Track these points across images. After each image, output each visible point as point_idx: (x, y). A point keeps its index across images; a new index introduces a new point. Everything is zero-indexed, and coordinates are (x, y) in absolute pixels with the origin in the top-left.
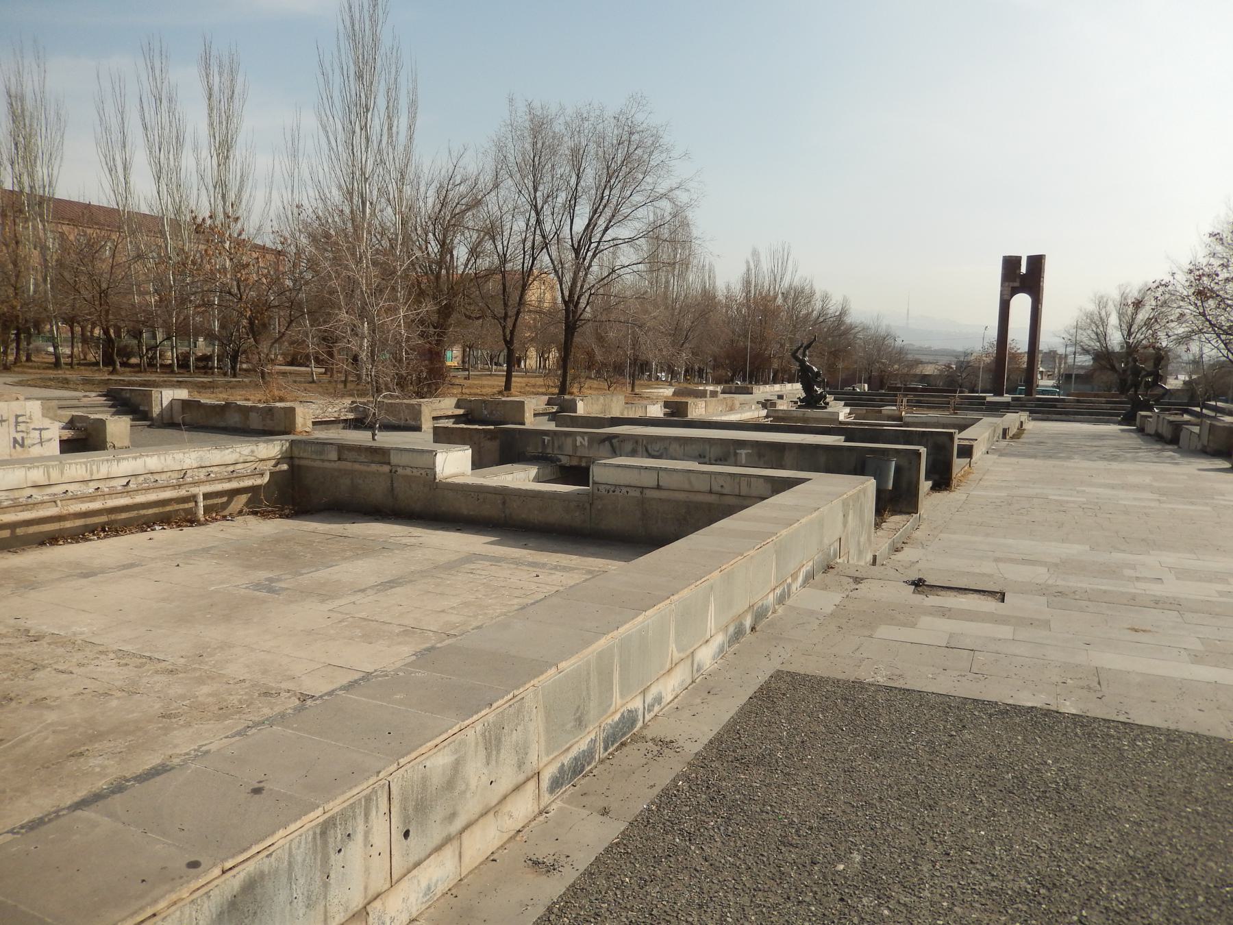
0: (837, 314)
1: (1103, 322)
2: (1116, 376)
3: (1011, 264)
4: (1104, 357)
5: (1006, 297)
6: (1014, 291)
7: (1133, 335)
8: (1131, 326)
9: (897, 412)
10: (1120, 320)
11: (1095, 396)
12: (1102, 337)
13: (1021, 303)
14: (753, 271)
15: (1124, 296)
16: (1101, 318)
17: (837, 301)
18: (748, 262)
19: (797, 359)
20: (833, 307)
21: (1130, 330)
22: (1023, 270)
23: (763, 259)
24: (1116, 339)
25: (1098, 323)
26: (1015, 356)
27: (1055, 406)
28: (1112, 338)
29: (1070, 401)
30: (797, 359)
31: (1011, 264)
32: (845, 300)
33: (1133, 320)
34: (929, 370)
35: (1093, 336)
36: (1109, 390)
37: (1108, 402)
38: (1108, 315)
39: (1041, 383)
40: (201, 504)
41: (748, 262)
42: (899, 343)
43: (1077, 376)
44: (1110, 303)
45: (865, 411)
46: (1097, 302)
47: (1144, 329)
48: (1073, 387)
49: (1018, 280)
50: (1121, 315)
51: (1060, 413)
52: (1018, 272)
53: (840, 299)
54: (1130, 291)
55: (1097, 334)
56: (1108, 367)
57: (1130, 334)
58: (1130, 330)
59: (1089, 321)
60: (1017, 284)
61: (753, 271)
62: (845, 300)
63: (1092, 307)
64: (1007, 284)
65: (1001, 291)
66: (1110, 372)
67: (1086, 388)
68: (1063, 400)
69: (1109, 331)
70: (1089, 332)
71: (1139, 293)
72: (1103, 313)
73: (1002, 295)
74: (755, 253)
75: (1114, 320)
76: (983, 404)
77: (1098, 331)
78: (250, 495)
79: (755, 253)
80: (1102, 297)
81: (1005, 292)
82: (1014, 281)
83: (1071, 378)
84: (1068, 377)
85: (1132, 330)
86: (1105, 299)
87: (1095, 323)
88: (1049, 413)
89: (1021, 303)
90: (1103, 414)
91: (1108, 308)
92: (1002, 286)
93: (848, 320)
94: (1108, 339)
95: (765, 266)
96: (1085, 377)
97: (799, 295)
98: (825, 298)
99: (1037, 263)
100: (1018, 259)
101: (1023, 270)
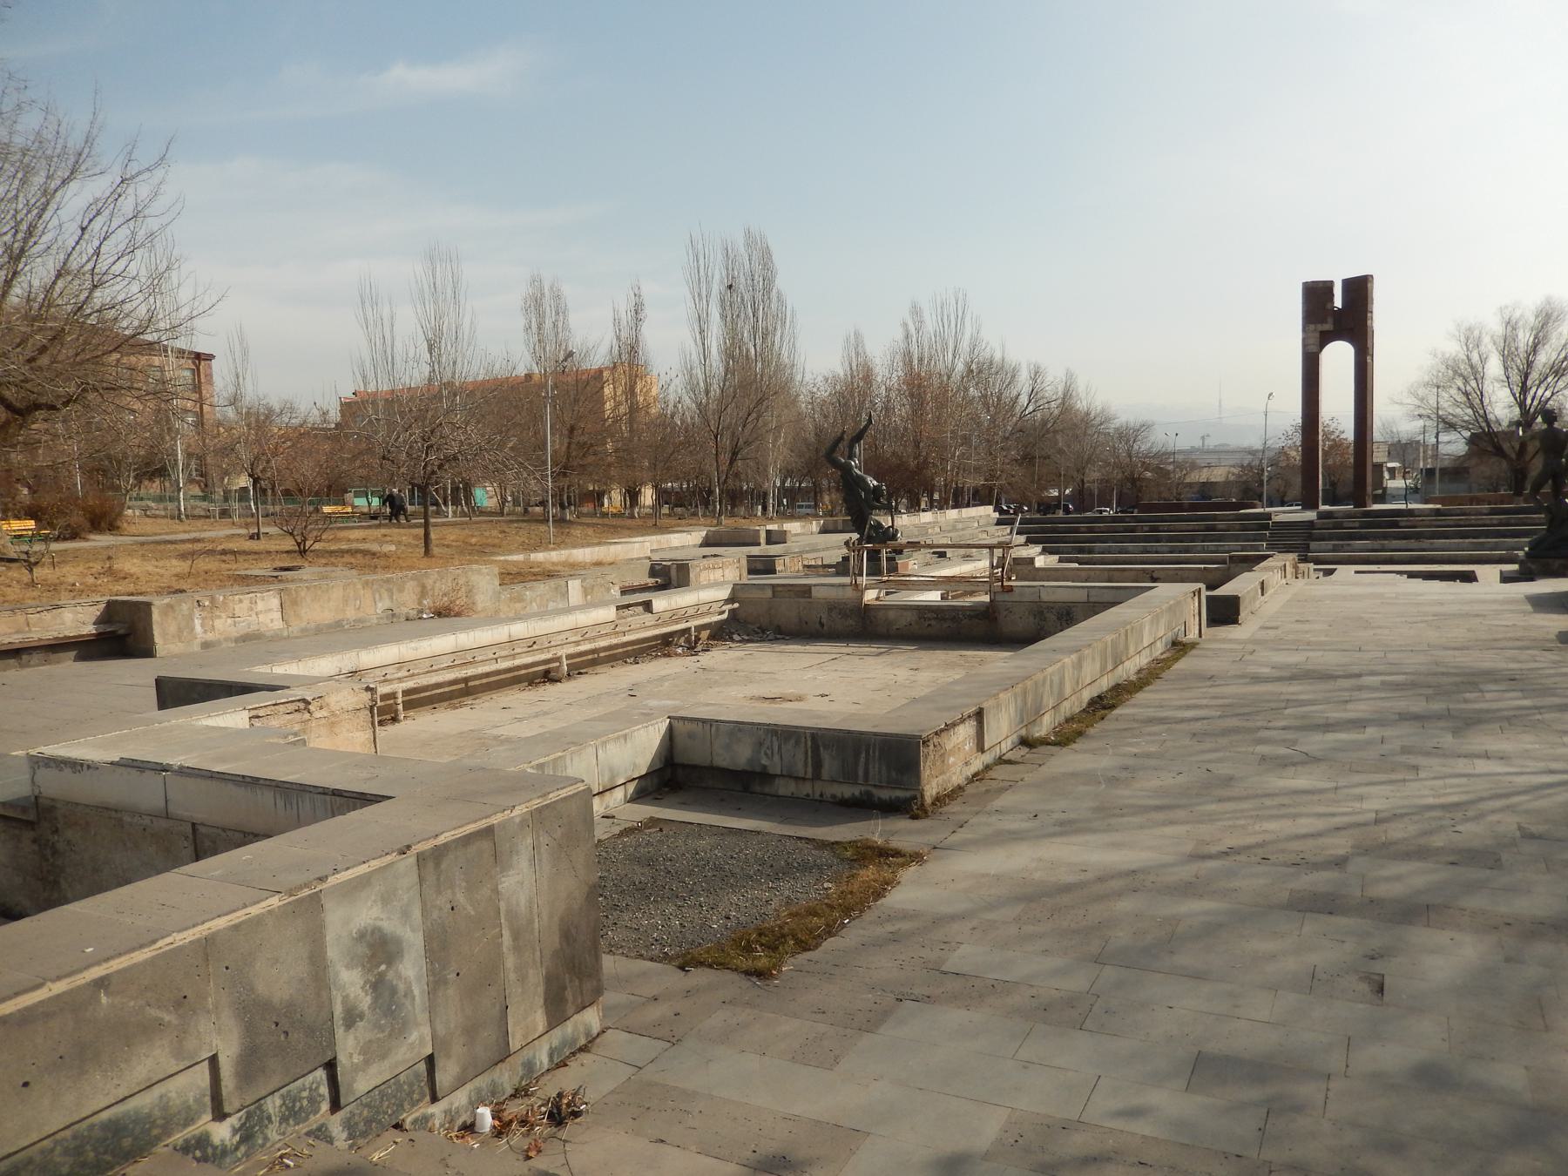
0: (1060, 394)
1: (1477, 373)
2: (1504, 464)
3: (1316, 295)
4: (1486, 441)
5: (1313, 349)
6: (1325, 339)
7: (1532, 392)
8: (1526, 376)
9: (849, 593)
10: (1506, 368)
11: (1472, 501)
12: (1475, 399)
13: (1338, 357)
14: (914, 339)
15: (1511, 325)
16: (1472, 367)
17: (1055, 378)
18: (905, 325)
19: (835, 463)
20: (1052, 386)
21: (1524, 383)
22: (1338, 302)
23: (927, 316)
24: (1502, 407)
25: (1467, 374)
26: (1337, 445)
27: (1396, 525)
28: (1493, 399)
29: (1421, 513)
30: (835, 463)
31: (1316, 295)
32: (1070, 375)
33: (1530, 364)
34: (1218, 475)
35: (1461, 398)
36: (1496, 490)
37: (1493, 512)
38: (1483, 360)
39: (188, 374)
40: (565, 662)
41: (905, 325)
42: (1116, 423)
43: (1443, 471)
44: (1486, 340)
45: (769, 593)
46: (1463, 339)
47: (1549, 379)
48: (1437, 488)
49: (1330, 320)
50: (1507, 357)
51: (1405, 537)
52: (1329, 306)
53: (1061, 375)
54: (1522, 316)
55: (1466, 394)
56: (1490, 449)
57: (1524, 389)
58: (1524, 383)
59: (1450, 372)
60: (1328, 327)
61: (914, 339)
62: (1070, 375)
63: (1454, 349)
64: (1312, 327)
65: (1304, 340)
66: (1494, 459)
67: (1460, 489)
68: (1410, 513)
69: (1488, 388)
70: (1453, 391)
71: (1537, 317)
72: (1475, 358)
73: (1305, 345)
74: (916, 311)
75: (1494, 367)
76: (1266, 527)
77: (1468, 388)
78: (1550, 482)
79: (916, 311)
80: (1470, 329)
81: (1311, 341)
82: (1323, 321)
83: (1434, 474)
84: (1430, 473)
85: (1529, 383)
86: (1476, 333)
87: (1461, 375)
88: (1385, 537)
89: (1338, 357)
90: (1487, 534)
91: (1482, 348)
92: (1304, 330)
93: (1081, 405)
94: (1486, 401)
95: (930, 326)
96: (1456, 472)
97: (979, 371)
98: (1036, 374)
99: (1359, 289)
100: (1327, 287)
101: (1338, 302)
